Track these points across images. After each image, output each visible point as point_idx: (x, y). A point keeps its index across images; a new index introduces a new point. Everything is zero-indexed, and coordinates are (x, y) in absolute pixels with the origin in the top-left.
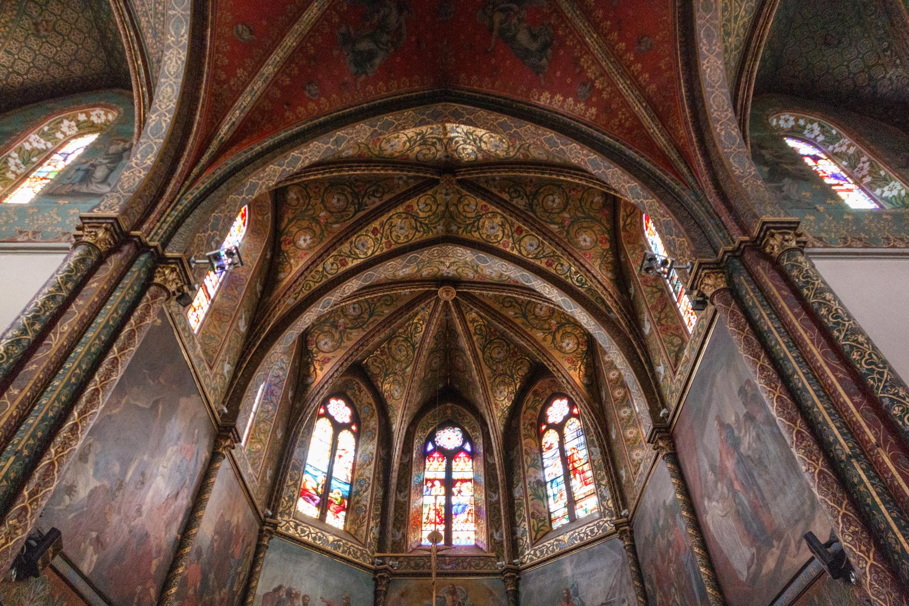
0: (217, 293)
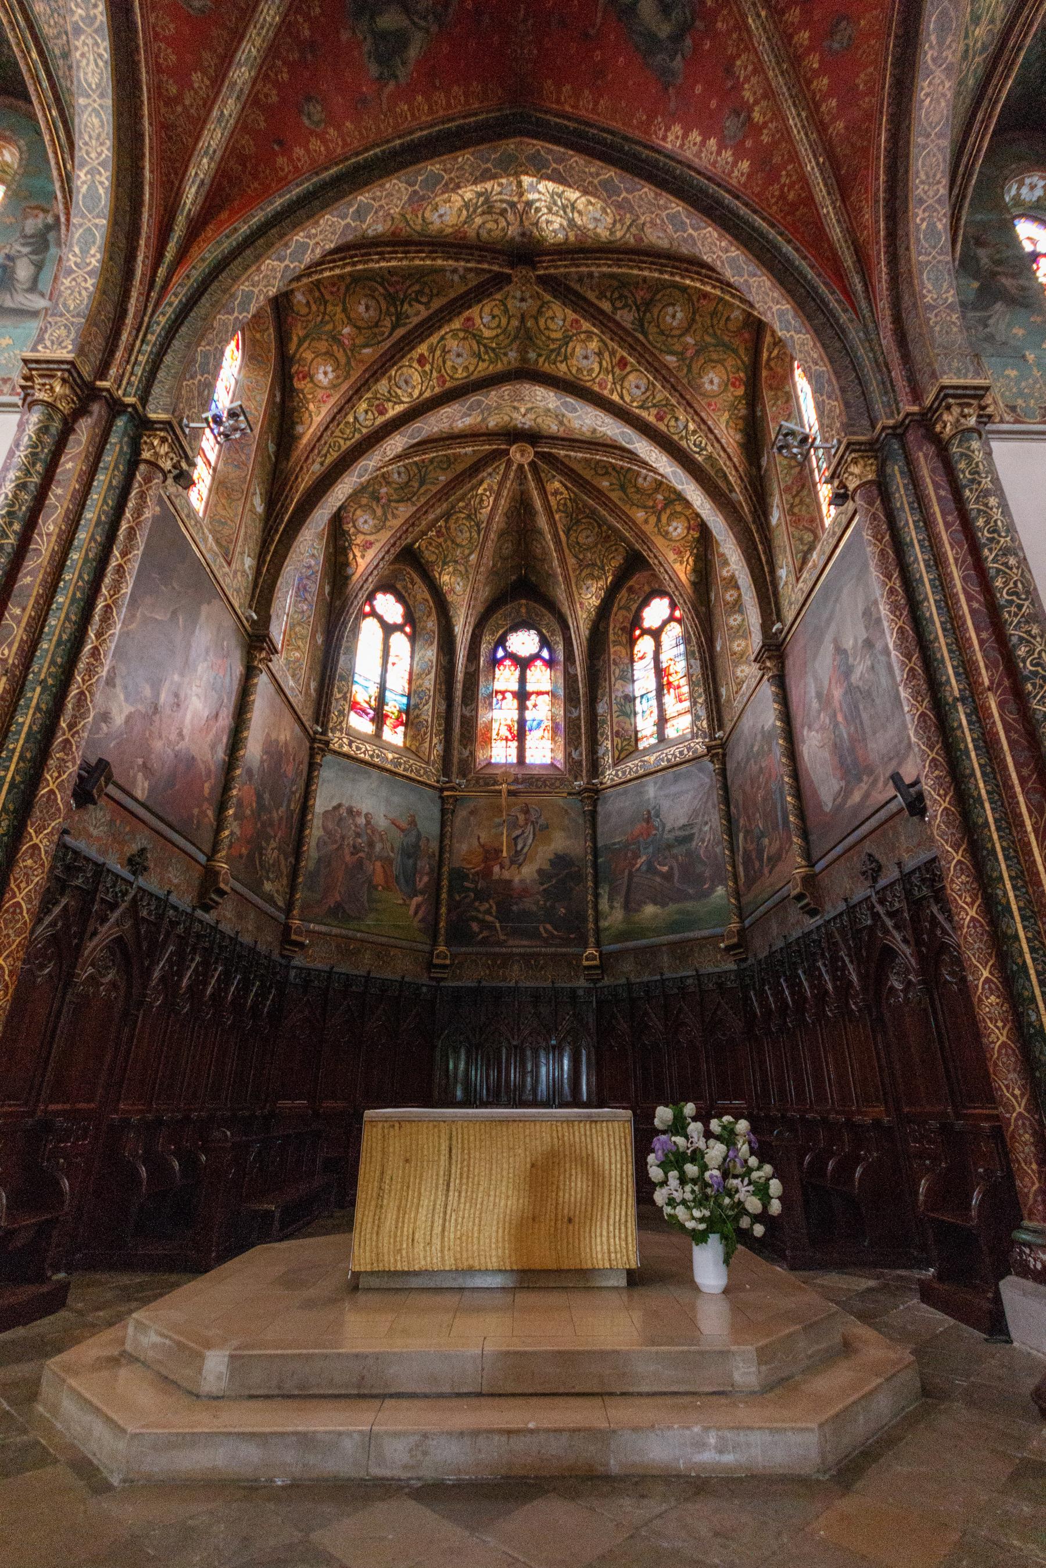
0: (218, 457)
